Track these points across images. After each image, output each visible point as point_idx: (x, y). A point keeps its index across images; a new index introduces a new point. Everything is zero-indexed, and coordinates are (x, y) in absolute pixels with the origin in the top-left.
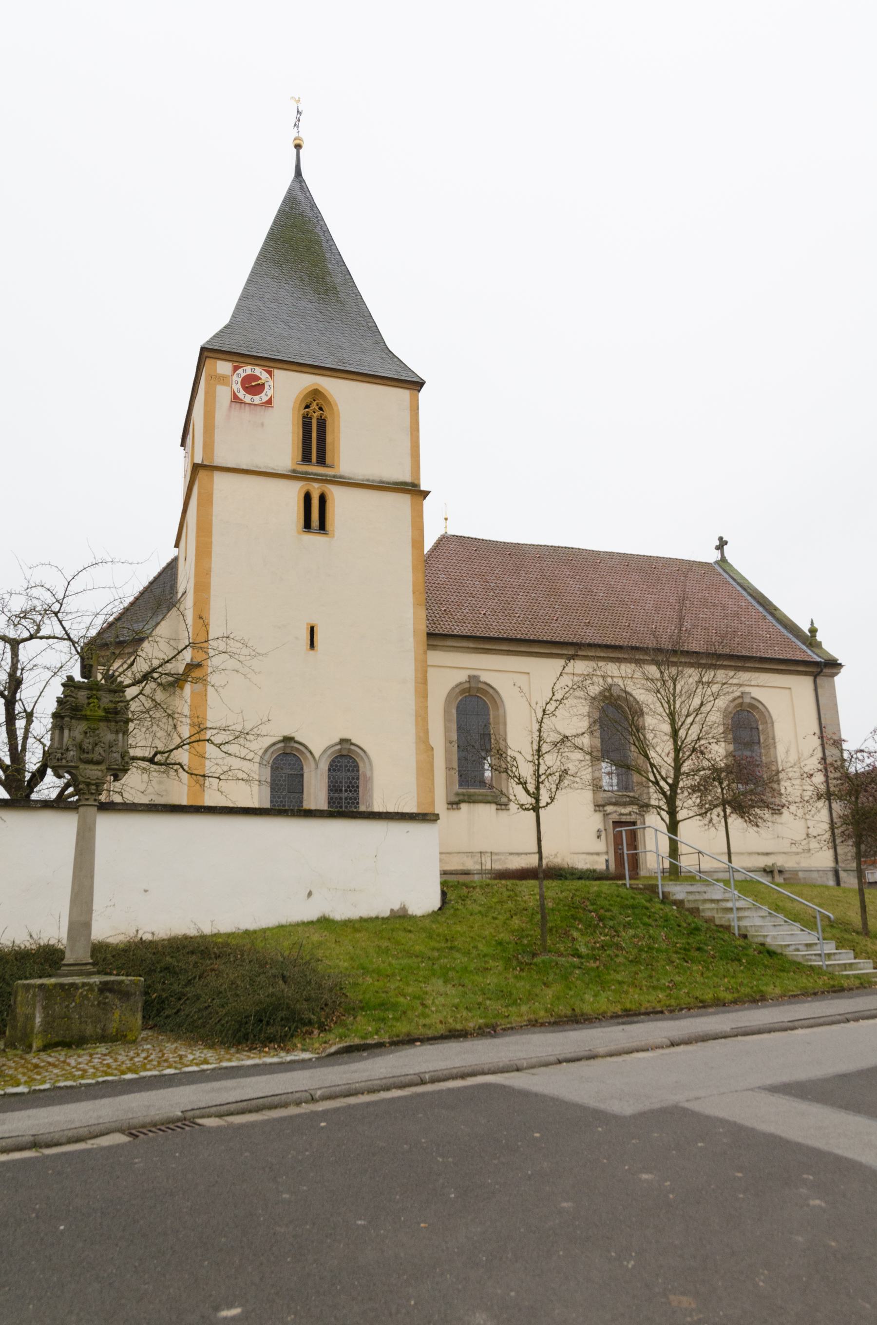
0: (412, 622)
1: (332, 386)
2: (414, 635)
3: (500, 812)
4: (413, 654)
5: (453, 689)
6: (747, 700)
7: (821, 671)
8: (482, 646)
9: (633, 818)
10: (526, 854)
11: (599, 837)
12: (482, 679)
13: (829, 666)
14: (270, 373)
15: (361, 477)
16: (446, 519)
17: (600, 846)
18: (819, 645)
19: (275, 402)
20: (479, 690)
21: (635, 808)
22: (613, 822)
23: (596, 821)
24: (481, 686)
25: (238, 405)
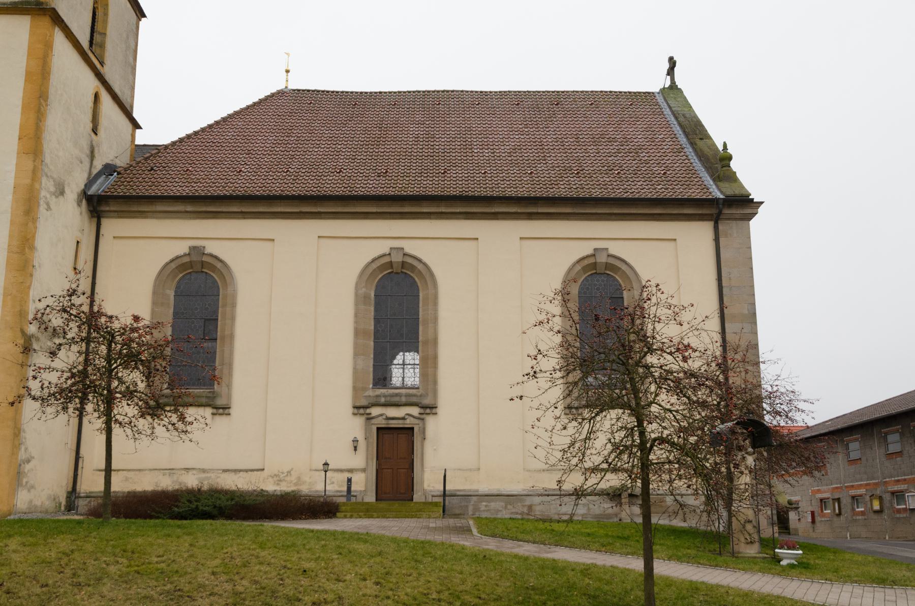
0: (13, 175)
2: (14, 192)
3: (217, 418)
4: (9, 215)
5: (167, 264)
6: (602, 259)
7: (720, 213)
9: (409, 422)
10: (246, 471)
11: (355, 448)
12: (208, 250)
13: (742, 205)
16: (287, 71)
17: (358, 460)
18: (732, 177)
21: (415, 411)
22: (378, 429)
23: (355, 427)
24: (205, 259)
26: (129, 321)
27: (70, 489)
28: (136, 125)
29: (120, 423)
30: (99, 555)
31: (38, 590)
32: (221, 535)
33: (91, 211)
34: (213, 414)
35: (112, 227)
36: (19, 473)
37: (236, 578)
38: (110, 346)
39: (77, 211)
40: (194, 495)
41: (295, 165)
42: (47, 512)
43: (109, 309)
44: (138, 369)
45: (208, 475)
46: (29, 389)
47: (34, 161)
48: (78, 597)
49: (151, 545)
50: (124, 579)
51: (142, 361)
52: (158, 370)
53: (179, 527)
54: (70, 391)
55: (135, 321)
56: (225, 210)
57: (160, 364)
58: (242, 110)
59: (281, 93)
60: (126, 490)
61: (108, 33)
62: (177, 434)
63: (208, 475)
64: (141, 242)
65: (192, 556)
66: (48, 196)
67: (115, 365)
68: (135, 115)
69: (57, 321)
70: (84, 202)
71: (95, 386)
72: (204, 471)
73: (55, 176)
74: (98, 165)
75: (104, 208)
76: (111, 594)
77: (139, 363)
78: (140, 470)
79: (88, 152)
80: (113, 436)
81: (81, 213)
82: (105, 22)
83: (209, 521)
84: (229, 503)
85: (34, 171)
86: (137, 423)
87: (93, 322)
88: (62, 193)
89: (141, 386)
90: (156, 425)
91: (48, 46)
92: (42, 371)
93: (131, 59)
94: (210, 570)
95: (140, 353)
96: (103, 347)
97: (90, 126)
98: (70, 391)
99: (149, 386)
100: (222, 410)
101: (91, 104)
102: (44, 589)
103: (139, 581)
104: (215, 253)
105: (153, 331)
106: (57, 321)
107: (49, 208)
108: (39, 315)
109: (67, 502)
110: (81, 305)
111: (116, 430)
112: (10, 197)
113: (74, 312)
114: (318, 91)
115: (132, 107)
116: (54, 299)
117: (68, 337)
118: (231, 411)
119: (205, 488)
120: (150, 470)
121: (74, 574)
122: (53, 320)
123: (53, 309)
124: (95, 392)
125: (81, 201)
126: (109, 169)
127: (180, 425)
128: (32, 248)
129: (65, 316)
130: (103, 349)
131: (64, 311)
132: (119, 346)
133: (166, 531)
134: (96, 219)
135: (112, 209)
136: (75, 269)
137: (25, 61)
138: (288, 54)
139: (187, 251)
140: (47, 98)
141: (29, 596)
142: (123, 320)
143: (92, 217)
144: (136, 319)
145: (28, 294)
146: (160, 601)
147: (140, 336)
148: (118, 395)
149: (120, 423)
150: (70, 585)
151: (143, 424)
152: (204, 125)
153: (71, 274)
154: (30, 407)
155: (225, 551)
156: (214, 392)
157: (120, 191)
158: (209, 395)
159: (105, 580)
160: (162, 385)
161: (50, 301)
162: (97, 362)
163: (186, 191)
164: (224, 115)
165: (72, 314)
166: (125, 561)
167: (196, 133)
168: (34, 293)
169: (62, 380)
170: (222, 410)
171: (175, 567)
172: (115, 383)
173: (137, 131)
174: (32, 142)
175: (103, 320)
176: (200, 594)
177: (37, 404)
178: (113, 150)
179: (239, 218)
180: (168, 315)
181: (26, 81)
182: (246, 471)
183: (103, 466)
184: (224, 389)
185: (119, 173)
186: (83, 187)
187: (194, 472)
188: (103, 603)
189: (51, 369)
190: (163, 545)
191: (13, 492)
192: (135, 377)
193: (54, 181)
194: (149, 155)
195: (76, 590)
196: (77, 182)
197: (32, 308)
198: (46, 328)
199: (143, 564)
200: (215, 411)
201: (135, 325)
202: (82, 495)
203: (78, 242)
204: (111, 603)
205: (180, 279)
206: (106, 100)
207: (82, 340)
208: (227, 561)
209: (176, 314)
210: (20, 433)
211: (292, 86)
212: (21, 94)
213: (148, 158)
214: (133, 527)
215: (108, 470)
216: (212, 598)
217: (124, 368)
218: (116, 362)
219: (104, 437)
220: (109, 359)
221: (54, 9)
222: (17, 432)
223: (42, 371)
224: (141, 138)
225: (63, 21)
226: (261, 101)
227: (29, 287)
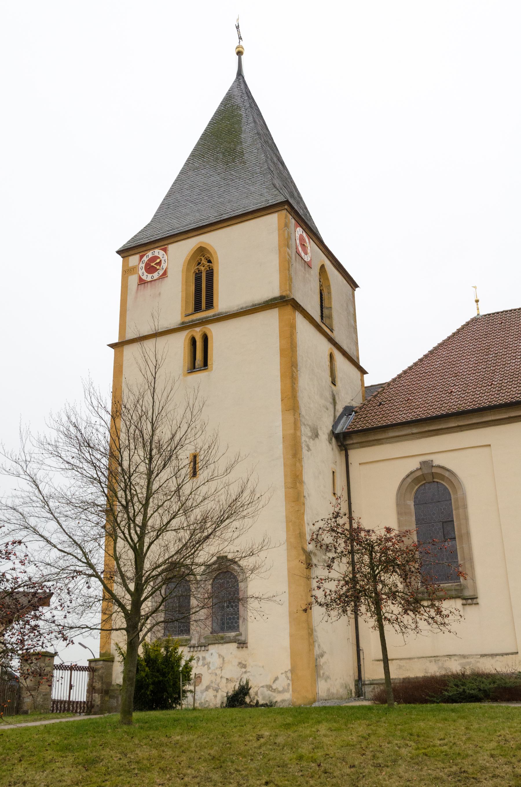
0: (281, 429)
1: (208, 239)
2: (283, 441)
3: (468, 608)
4: (282, 459)
5: (404, 479)
8: (427, 429)
10: (502, 655)
14: (165, 250)
15: (236, 308)
16: (477, 301)
19: (169, 273)
20: (433, 475)
24: (434, 470)
25: (143, 286)
26: (383, 532)
27: (357, 678)
28: (363, 372)
29: (389, 620)
30: (391, 738)
31: (348, 771)
32: (492, 718)
33: (339, 446)
34: (463, 605)
35: (357, 455)
36: (316, 666)
37: (514, 760)
38: (371, 555)
39: (329, 447)
40: (460, 679)
41: (497, 377)
42: (342, 698)
43: (366, 525)
44: (396, 572)
45: (469, 660)
46: (316, 598)
47: (294, 415)
48: (380, 777)
49: (432, 728)
50: (415, 761)
51: (398, 565)
52: (413, 572)
53: (453, 710)
54: (347, 597)
55: (388, 532)
56: (443, 426)
57: (414, 566)
58: (444, 342)
59: (474, 321)
60: (401, 677)
61: (333, 306)
62: (437, 626)
63: (469, 660)
64: (381, 464)
65: (469, 739)
66: (307, 440)
67: (377, 571)
68: (362, 364)
69: (327, 539)
70: (333, 439)
71: (365, 590)
72: (464, 657)
73: (310, 424)
74: (340, 409)
75: (349, 442)
76: (406, 774)
77: (396, 567)
78: (410, 659)
79: (331, 400)
80: (385, 632)
81: (332, 449)
82: (330, 298)
83: (477, 704)
84: (492, 686)
85: (295, 423)
86: (402, 619)
87: (354, 535)
88: (317, 436)
89: (401, 587)
90: (418, 620)
91: (293, 327)
92: (323, 582)
93: (352, 322)
94: (488, 752)
95: (395, 559)
96: (366, 556)
97: (330, 379)
98: (347, 597)
99: (407, 586)
100: (471, 600)
101: (328, 363)
102: (352, 769)
103: (428, 763)
104: (442, 464)
105: (403, 539)
106: (327, 539)
107: (309, 449)
108: (315, 537)
109: (356, 689)
110: (344, 524)
111: (387, 627)
112: (281, 445)
113: (340, 530)
114: (507, 311)
115: (358, 358)
116: (324, 522)
117: (338, 551)
118: (479, 601)
119: (468, 672)
120: (419, 658)
121: (374, 756)
122: (325, 539)
123: (324, 530)
124: (366, 595)
125: (331, 439)
126: (348, 410)
127: (438, 618)
128: (302, 482)
129: (334, 534)
130: (366, 558)
131: (333, 530)
132: (379, 555)
133: (442, 716)
134: (344, 452)
135: (355, 441)
136: (334, 494)
137: (279, 342)
138: (475, 287)
139: (419, 466)
140: (297, 365)
141: (342, 776)
142: (378, 533)
143: (341, 450)
144: (388, 530)
145: (303, 519)
146: (449, 782)
147: (393, 544)
148: (384, 597)
149: (389, 620)
150: (372, 766)
151: (408, 619)
152: (416, 360)
153: (333, 499)
154: (318, 611)
155: (499, 734)
156: (461, 585)
157: (359, 426)
158: (457, 588)
159: (400, 762)
160: (417, 583)
161: (321, 524)
162: (363, 570)
163: (410, 417)
164: (431, 348)
165: (338, 533)
166: (413, 744)
167: (410, 368)
168: (307, 518)
169: (339, 587)
170: (471, 600)
171: (457, 749)
172: (380, 586)
173: (365, 375)
174: (291, 402)
175: (363, 534)
176: (484, 776)
177: (324, 609)
178: (349, 396)
179: (457, 432)
180: (413, 526)
181: (281, 356)
182: (502, 655)
183: (381, 657)
184: (469, 582)
185: (356, 412)
186: (331, 428)
187: (456, 658)
188: (401, 784)
189: (328, 579)
190: (442, 729)
191: (315, 682)
192: (393, 579)
193: (310, 428)
194: (376, 394)
195: (378, 771)
196: (326, 425)
197: (309, 530)
198: (321, 546)
199: (429, 746)
200: (464, 602)
201: (388, 536)
202: (367, 682)
203: (333, 472)
204: (408, 783)
205: (417, 490)
206: (338, 357)
207: (349, 552)
208: (502, 743)
209: (418, 521)
210: (312, 632)
211: (483, 313)
212: (279, 367)
213: (376, 395)
214: (414, 712)
215: (386, 660)
216: (495, 780)
217: (385, 573)
218: (378, 568)
219: (378, 633)
220: (372, 566)
221: (293, 299)
222: (311, 632)
223: (323, 582)
224: (369, 381)
225: (300, 306)
226: (459, 331)
227: (303, 514)
